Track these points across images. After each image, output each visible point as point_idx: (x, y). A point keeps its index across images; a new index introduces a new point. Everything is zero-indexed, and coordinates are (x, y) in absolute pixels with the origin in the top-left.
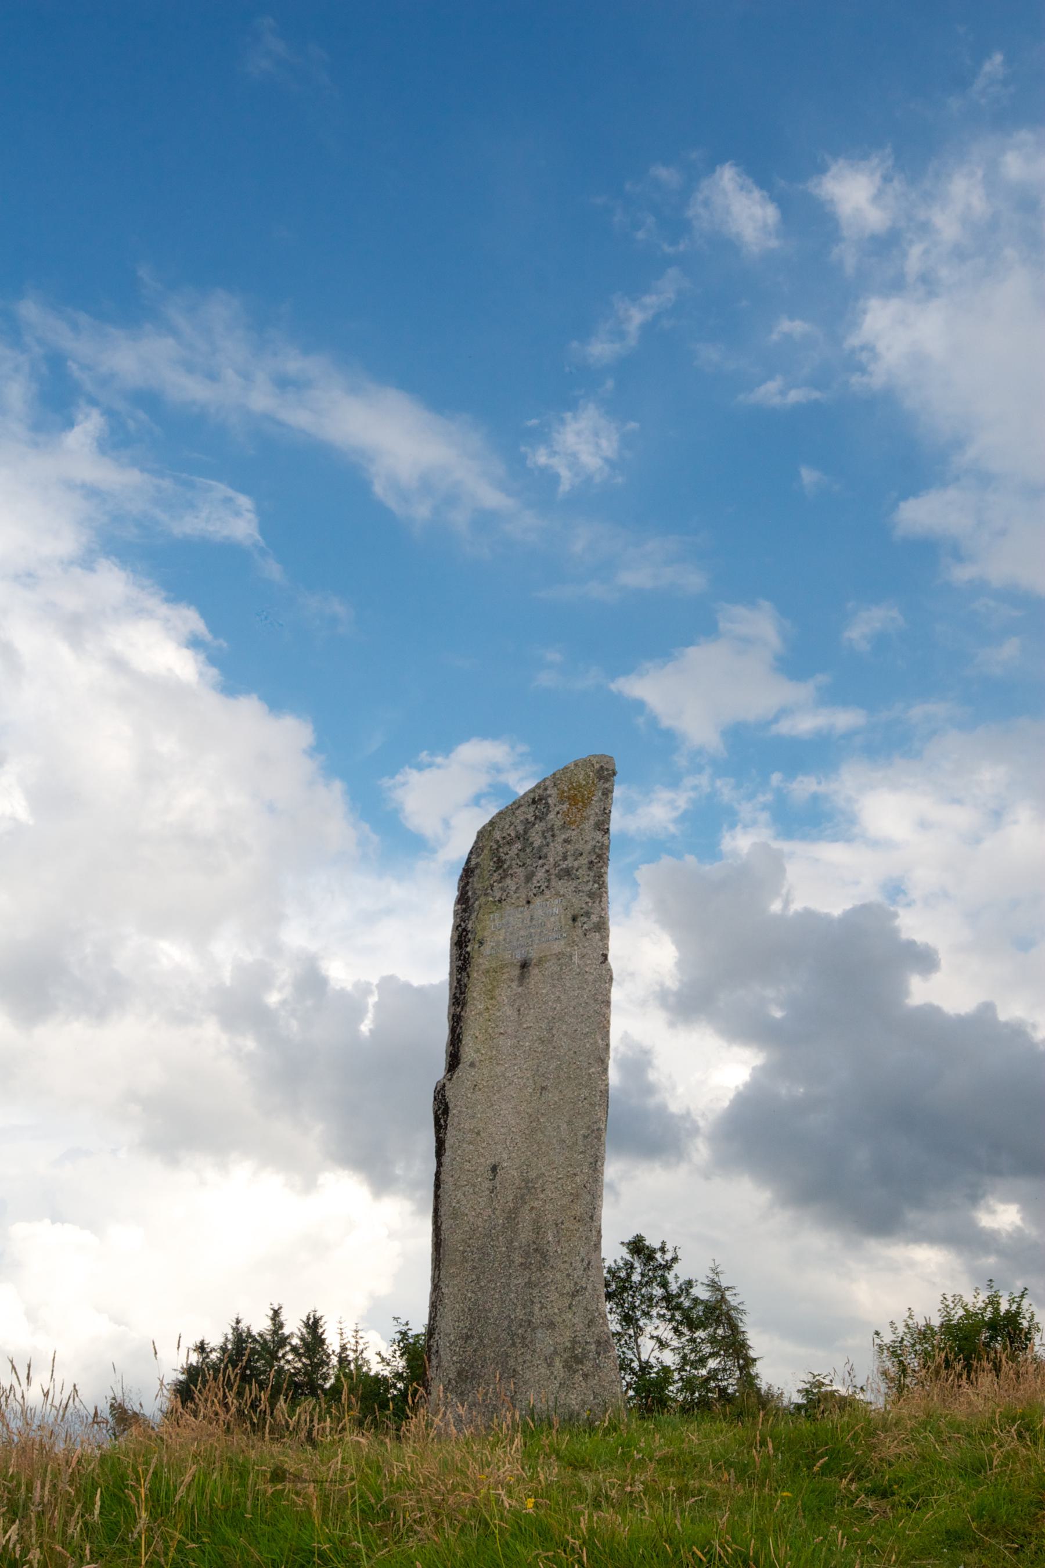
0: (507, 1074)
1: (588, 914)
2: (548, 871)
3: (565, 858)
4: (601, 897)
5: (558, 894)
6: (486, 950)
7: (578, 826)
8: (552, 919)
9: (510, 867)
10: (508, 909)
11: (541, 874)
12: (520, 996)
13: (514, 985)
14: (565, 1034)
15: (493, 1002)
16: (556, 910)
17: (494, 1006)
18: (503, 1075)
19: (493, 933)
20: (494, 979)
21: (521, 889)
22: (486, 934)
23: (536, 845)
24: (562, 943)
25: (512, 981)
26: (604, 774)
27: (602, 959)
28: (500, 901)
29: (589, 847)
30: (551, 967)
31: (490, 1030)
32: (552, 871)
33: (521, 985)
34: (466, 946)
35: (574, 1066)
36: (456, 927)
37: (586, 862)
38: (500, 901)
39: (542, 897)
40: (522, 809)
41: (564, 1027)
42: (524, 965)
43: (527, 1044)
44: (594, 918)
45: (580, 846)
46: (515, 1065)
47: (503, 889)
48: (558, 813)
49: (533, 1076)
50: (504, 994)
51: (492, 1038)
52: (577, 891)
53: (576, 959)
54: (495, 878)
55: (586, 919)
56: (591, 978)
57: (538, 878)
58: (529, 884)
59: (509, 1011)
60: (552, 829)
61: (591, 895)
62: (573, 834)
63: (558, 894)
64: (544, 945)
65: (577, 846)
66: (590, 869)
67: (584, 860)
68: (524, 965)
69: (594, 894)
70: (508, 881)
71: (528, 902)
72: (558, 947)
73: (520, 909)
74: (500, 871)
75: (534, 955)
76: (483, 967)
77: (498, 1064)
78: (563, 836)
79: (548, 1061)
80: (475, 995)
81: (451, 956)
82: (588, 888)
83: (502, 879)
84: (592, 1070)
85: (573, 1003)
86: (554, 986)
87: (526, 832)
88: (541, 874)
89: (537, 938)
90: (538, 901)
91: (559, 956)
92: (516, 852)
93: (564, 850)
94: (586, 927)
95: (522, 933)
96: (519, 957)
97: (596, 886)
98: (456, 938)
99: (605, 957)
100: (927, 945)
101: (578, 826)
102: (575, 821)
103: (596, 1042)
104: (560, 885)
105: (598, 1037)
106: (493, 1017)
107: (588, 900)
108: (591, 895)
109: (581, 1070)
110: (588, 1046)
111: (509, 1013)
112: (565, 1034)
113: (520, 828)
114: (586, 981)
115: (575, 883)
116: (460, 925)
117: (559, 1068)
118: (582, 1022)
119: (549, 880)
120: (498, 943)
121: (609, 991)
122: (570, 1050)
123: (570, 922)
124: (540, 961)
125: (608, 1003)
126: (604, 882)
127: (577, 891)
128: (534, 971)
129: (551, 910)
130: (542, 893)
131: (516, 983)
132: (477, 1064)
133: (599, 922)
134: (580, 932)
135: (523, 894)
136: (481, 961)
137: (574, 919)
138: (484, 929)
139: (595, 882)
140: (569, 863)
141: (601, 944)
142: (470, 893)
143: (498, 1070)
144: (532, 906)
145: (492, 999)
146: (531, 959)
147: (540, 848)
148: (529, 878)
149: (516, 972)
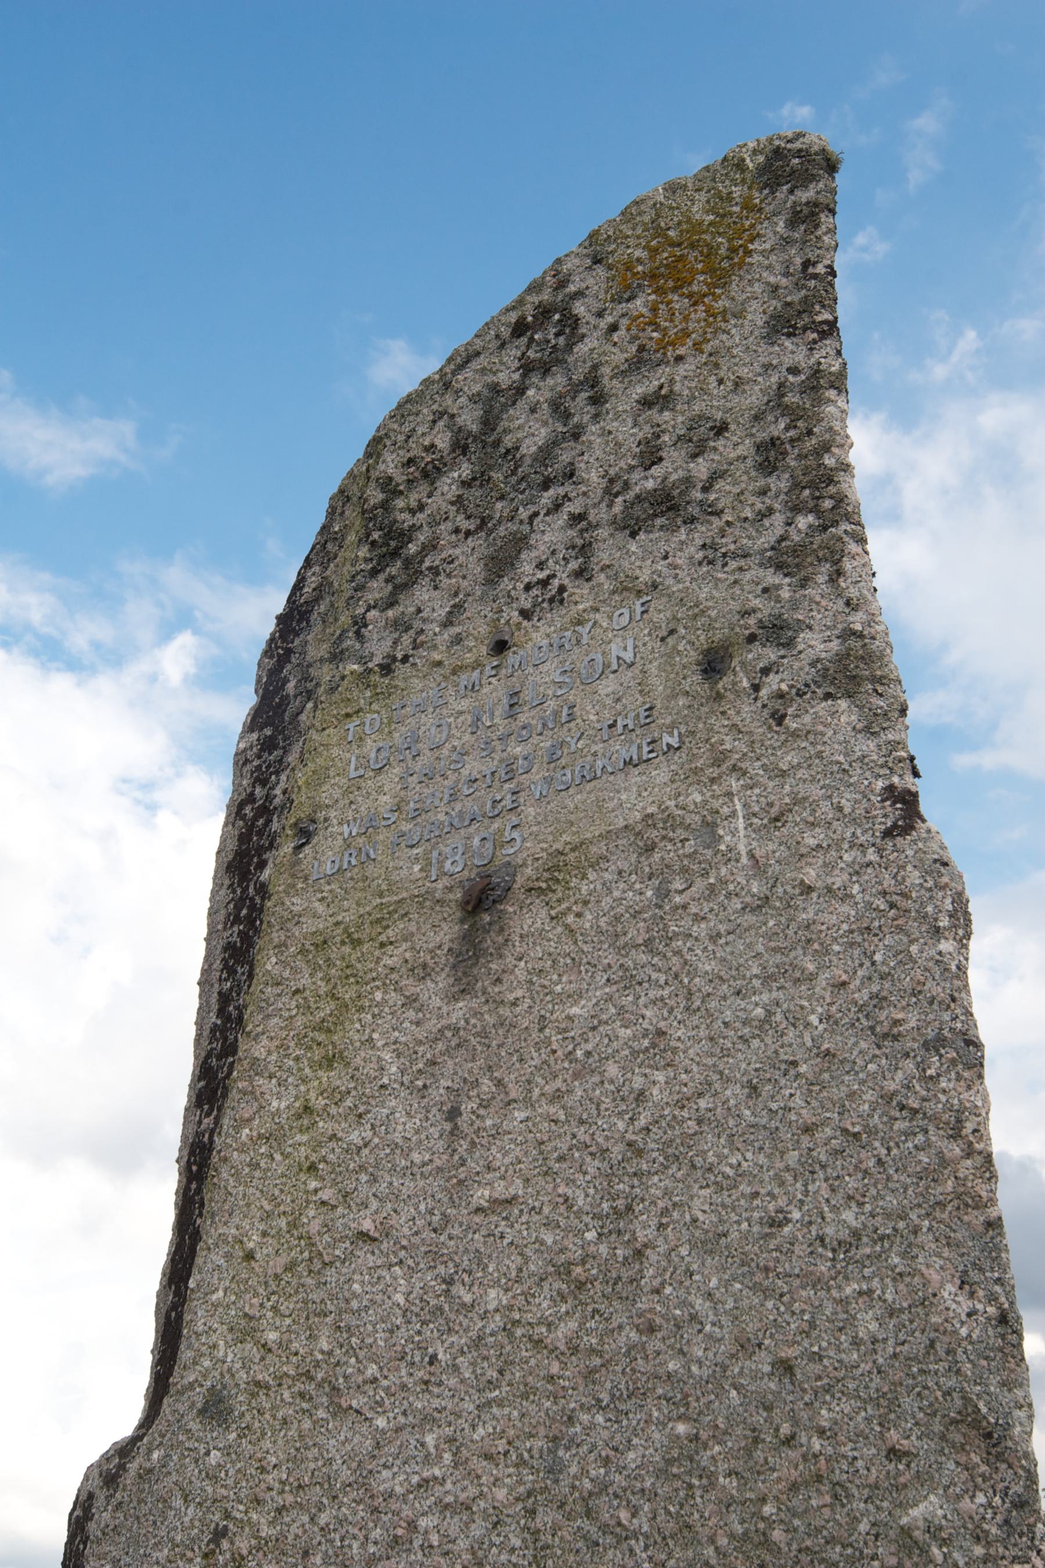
0: (387, 1480)
1: (779, 632)
2: (577, 518)
3: (650, 455)
4: (835, 556)
5: (628, 588)
6: (325, 855)
7: (697, 347)
8: (608, 686)
9: (431, 546)
10: (415, 685)
11: (552, 535)
12: (455, 1039)
13: (432, 992)
14: (710, 1243)
15: (337, 1078)
16: (620, 649)
17: (336, 1095)
18: (363, 1481)
19: (355, 785)
20: (349, 974)
21: (472, 608)
22: (327, 793)
23: (529, 448)
24: (660, 774)
25: (423, 972)
26: (795, 176)
27: (889, 814)
28: (386, 669)
29: (754, 398)
30: (612, 891)
31: (313, 1221)
32: (600, 514)
33: (463, 989)
34: (262, 865)
35: (787, 1466)
36: (237, 810)
37: (746, 448)
38: (386, 669)
39: (559, 617)
40: (482, 361)
41: (701, 1203)
42: (482, 899)
43: (494, 1297)
44: (817, 644)
45: (715, 403)
46: (428, 1420)
47: (401, 625)
48: (614, 328)
49: (529, 1502)
50: (383, 1041)
51: (320, 1263)
52: (712, 555)
53: (738, 836)
54: (371, 597)
55: (771, 654)
56: (838, 916)
57: (541, 551)
58: (506, 584)
59: (404, 1119)
60: (592, 380)
61: (786, 559)
62: (682, 375)
63: (628, 588)
64: (575, 799)
65: (697, 407)
66: (767, 467)
67: (736, 448)
68: (482, 899)
69: (798, 550)
70: (421, 593)
71: (500, 647)
72: (633, 798)
73: (464, 679)
74: (394, 569)
75: (527, 847)
76: (309, 925)
77: (339, 1411)
78: (639, 390)
79: (613, 1408)
80: (259, 1051)
81: (212, 913)
82: (766, 539)
83: (400, 588)
84: (926, 1508)
85: (745, 1062)
86: (630, 981)
87: (489, 423)
88: (552, 535)
89: (538, 774)
90: (539, 634)
91: (646, 836)
92: (455, 490)
93: (647, 431)
94: (773, 683)
95: (473, 767)
96: (458, 861)
97: (804, 522)
98: (232, 845)
99: (907, 802)
100: (152, 1352)
101: (697, 347)
102: (686, 334)
103: (927, 1302)
104: (638, 557)
105: (938, 1273)
106: (332, 1153)
107: (772, 578)
108: (786, 559)
109: (839, 1495)
110: (868, 1324)
111: (404, 1127)
112: (710, 1243)
113: (469, 419)
114: (809, 937)
115: (702, 533)
116: (251, 798)
117: (682, 1461)
118: (809, 1168)
119: (585, 550)
120: (370, 828)
121: (958, 975)
122: (746, 1346)
123: (694, 680)
124: (556, 873)
125: (967, 1052)
126: (840, 500)
127: (712, 555)
128: (527, 920)
129: (607, 652)
130: (559, 598)
131: (443, 980)
132: (240, 1402)
133: (842, 658)
134: (747, 712)
135: (478, 626)
136: (297, 903)
137: (713, 664)
138: (320, 778)
139: (796, 509)
140: (673, 466)
141: (867, 746)
142: (291, 686)
143: (342, 1442)
144: (512, 658)
145: (329, 1062)
146: (512, 868)
147: (546, 454)
148: (500, 565)
149: (444, 933)
